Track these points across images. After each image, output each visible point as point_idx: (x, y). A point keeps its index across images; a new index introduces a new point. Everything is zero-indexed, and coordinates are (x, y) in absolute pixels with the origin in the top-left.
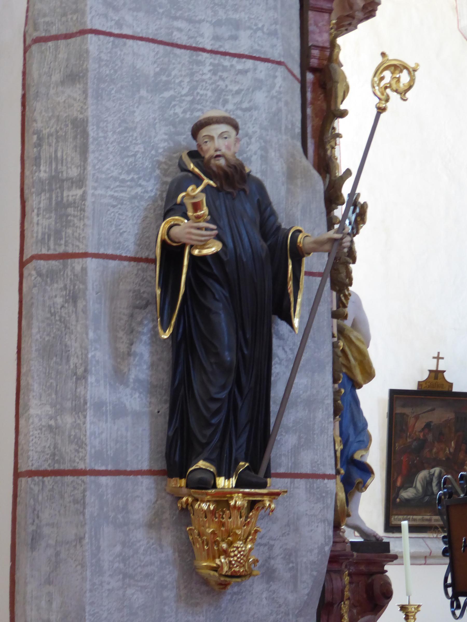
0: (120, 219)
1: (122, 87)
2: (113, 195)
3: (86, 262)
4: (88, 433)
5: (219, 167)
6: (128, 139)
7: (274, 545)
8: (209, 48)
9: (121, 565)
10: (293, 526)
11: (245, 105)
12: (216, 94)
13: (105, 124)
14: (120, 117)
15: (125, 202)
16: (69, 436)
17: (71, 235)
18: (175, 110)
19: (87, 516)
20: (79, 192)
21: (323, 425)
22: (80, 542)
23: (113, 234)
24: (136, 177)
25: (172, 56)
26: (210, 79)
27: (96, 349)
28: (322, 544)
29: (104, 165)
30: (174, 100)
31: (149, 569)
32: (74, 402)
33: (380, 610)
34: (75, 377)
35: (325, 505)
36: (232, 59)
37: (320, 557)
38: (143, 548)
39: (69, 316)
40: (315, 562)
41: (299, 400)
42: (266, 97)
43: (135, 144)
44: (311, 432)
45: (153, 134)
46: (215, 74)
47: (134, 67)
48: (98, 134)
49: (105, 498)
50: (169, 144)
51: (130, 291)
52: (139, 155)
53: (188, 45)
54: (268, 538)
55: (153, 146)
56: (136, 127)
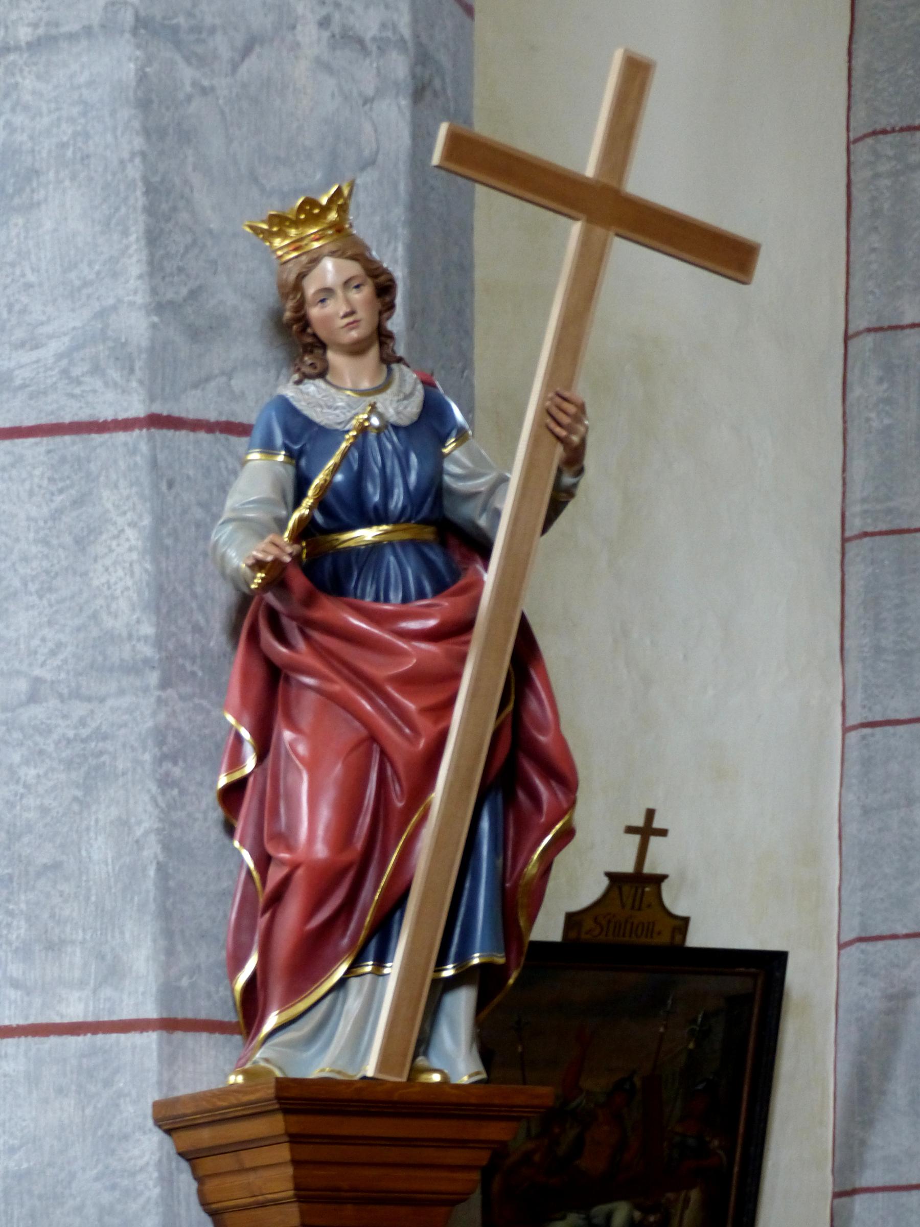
33: (329, 970)
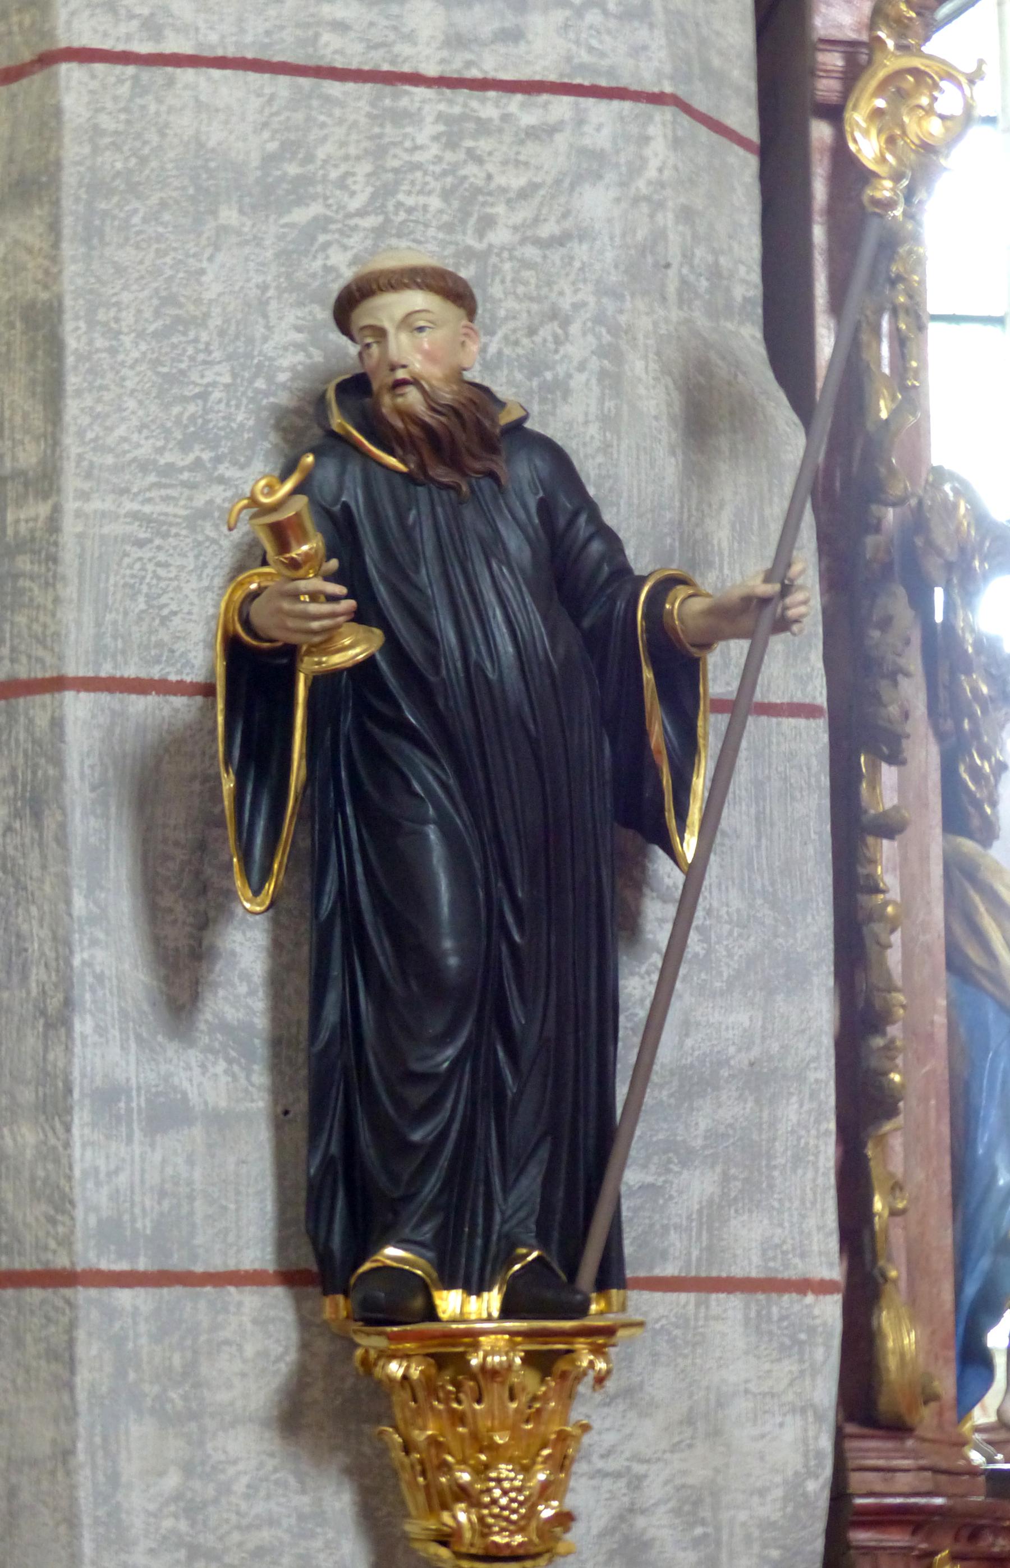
0: (159, 579)
1: (163, 204)
2: (139, 511)
3: (61, 704)
4: (77, 1173)
5: (407, 415)
6: (184, 350)
7: (645, 1476)
8: (431, 70)
9: (183, 1526)
10: (703, 1422)
11: (548, 229)
12: (456, 204)
13: (112, 313)
14: (157, 290)
15: (174, 530)
16: (33, 1180)
17: (25, 632)
18: (327, 257)
19: (81, 1396)
20: (43, 510)
21: (803, 1141)
22: (65, 1462)
23: (140, 619)
24: (206, 456)
25: (315, 103)
26: (438, 159)
27: (94, 942)
28: (796, 1474)
29: (109, 430)
30: (325, 230)
31: (265, 1535)
32: (40, 1089)
34: (42, 1021)
35: (807, 1365)
36: (504, 97)
37: (789, 1509)
38: (245, 1480)
39: (24, 855)
40: (775, 1523)
41: (725, 1073)
42: (618, 200)
43: (205, 362)
44: (764, 1163)
45: (260, 331)
46: (451, 143)
47: (201, 145)
48: (90, 342)
49: (130, 1346)
50: (309, 356)
51: (193, 778)
52: (217, 394)
53: (366, 68)
54: (627, 1454)
55: (259, 366)
56: (206, 315)
